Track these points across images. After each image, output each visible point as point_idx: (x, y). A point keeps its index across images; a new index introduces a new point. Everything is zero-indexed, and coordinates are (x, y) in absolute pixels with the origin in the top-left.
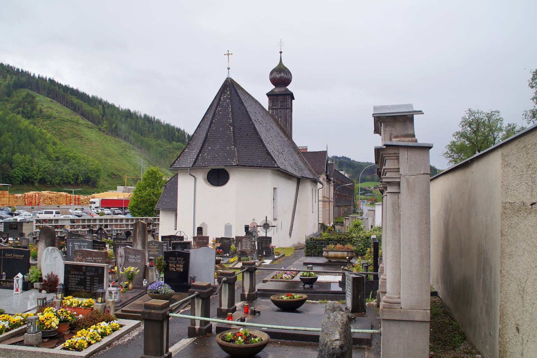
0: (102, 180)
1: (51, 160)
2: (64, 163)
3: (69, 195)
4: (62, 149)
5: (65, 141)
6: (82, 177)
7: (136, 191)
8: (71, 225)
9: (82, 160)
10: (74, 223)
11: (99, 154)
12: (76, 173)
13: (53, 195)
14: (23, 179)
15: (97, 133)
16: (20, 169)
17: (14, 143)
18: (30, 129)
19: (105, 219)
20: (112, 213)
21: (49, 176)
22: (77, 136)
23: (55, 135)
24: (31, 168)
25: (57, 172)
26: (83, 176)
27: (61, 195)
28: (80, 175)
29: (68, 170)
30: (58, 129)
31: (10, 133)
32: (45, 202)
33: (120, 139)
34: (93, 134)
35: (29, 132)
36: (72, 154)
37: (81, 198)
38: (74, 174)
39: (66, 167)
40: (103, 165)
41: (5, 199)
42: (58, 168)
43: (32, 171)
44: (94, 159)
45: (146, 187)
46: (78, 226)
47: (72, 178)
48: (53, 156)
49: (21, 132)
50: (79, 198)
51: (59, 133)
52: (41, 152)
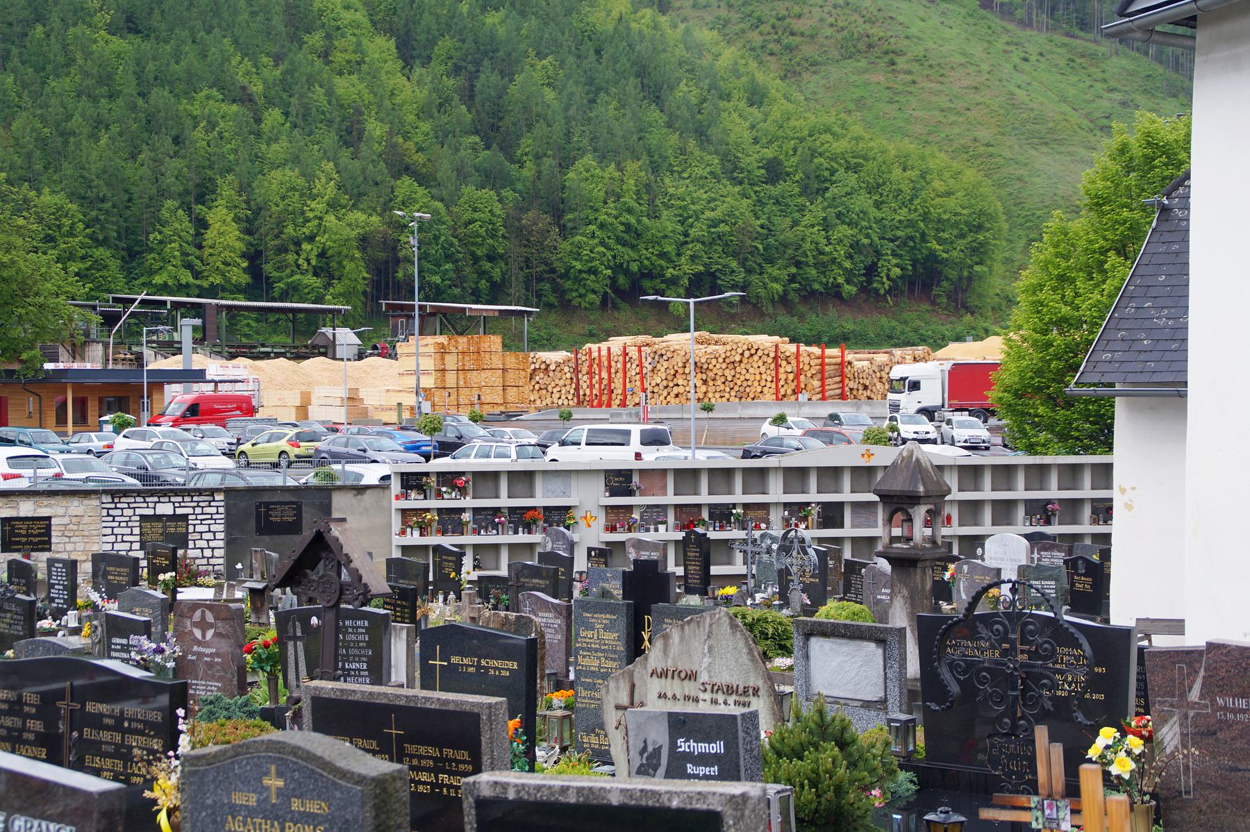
0: (999, 268)
1: (741, 183)
2: (805, 191)
3: (792, 348)
4: (793, 123)
5: (812, 82)
6: (894, 261)
7: (1041, 287)
8: (609, 509)
9: (897, 172)
10: (630, 493)
11: (984, 134)
12: (866, 241)
13: (711, 348)
14: (613, 280)
15: (970, 20)
16: (598, 233)
17: (567, 109)
18: (640, 33)
19: (819, 469)
20: (999, 440)
21: (734, 264)
22: (870, 46)
23: (759, 53)
24: (648, 229)
25: (771, 240)
26: (900, 256)
27: (753, 351)
28: (888, 247)
29: (826, 226)
30: (773, 21)
31: (550, 58)
32: (676, 390)
33: (1095, 41)
34: (955, 31)
35: (638, 48)
36: (840, 146)
37: (858, 365)
38: (855, 245)
39: (816, 211)
40: (1003, 192)
41: (484, 374)
42: (777, 220)
43: (655, 242)
44: (955, 164)
45: (1104, 252)
46: (655, 515)
47: (847, 264)
48: (752, 159)
49: (598, 52)
50: (843, 365)
51: (778, 41)
52: (692, 144)
